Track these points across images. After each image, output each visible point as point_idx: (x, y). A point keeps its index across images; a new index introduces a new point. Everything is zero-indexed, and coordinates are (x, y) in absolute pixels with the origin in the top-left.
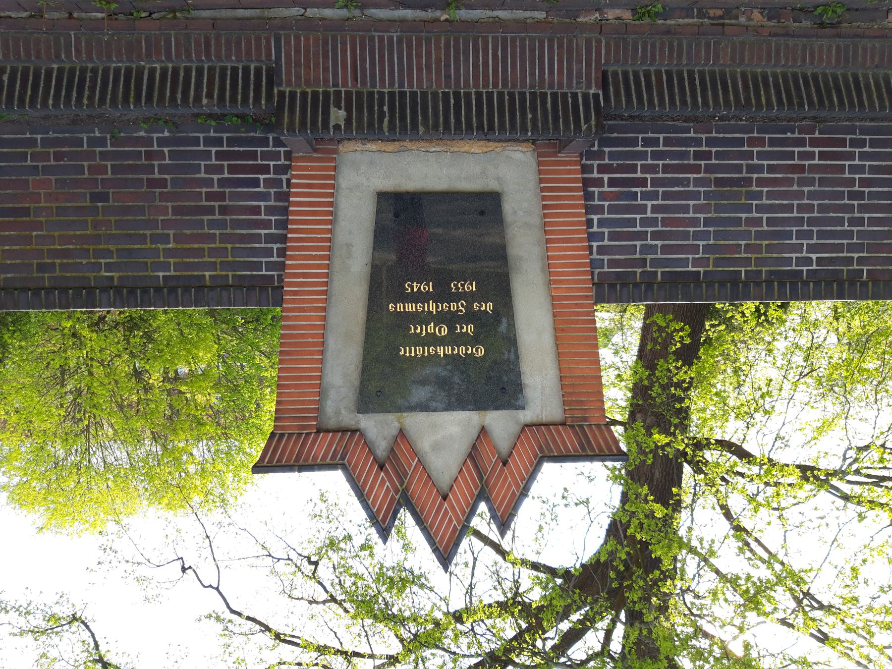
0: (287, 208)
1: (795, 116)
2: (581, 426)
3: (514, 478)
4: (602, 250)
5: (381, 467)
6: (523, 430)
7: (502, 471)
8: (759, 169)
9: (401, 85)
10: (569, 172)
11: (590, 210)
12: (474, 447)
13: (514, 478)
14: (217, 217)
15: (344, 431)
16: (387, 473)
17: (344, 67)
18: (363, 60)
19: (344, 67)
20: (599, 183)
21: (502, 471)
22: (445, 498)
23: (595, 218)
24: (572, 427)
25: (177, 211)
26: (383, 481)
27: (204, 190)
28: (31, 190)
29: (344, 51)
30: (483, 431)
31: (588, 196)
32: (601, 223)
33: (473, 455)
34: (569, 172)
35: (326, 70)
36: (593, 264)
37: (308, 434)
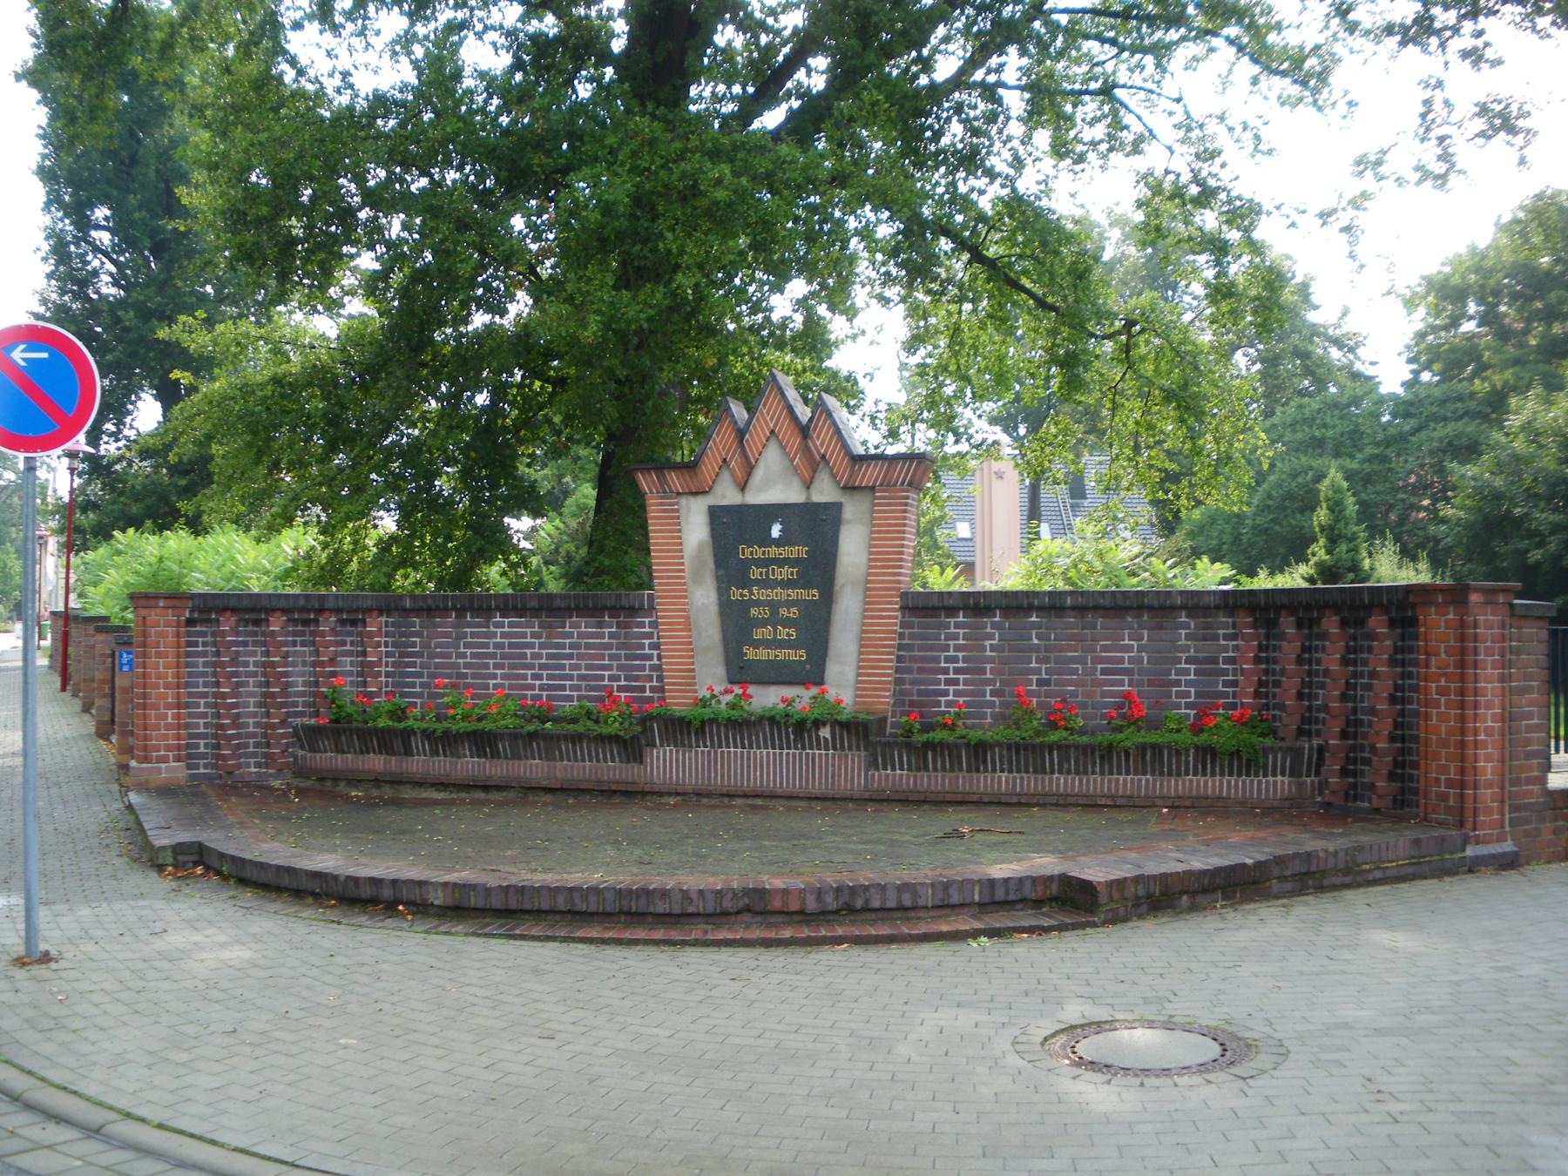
0: (897, 672)
1: (1443, 334)
2: (665, 492)
3: (718, 449)
4: (650, 636)
5: (823, 457)
6: (711, 488)
7: (727, 454)
8: (573, 688)
9: (781, 754)
10: (674, 698)
11: (658, 668)
12: (749, 474)
13: (718, 449)
14: (951, 666)
15: (854, 488)
16: (818, 452)
17: (820, 766)
18: (807, 771)
19: (820, 766)
20: (653, 689)
21: (727, 454)
22: (772, 432)
23: (655, 662)
24: (671, 492)
25: (487, 687)
26: (822, 444)
27: (961, 687)
28: (1193, 690)
29: (820, 778)
30: (743, 488)
31: (660, 679)
32: (650, 657)
33: (750, 468)
34: (674, 698)
35: (833, 766)
36: (654, 625)
37: (881, 485)
